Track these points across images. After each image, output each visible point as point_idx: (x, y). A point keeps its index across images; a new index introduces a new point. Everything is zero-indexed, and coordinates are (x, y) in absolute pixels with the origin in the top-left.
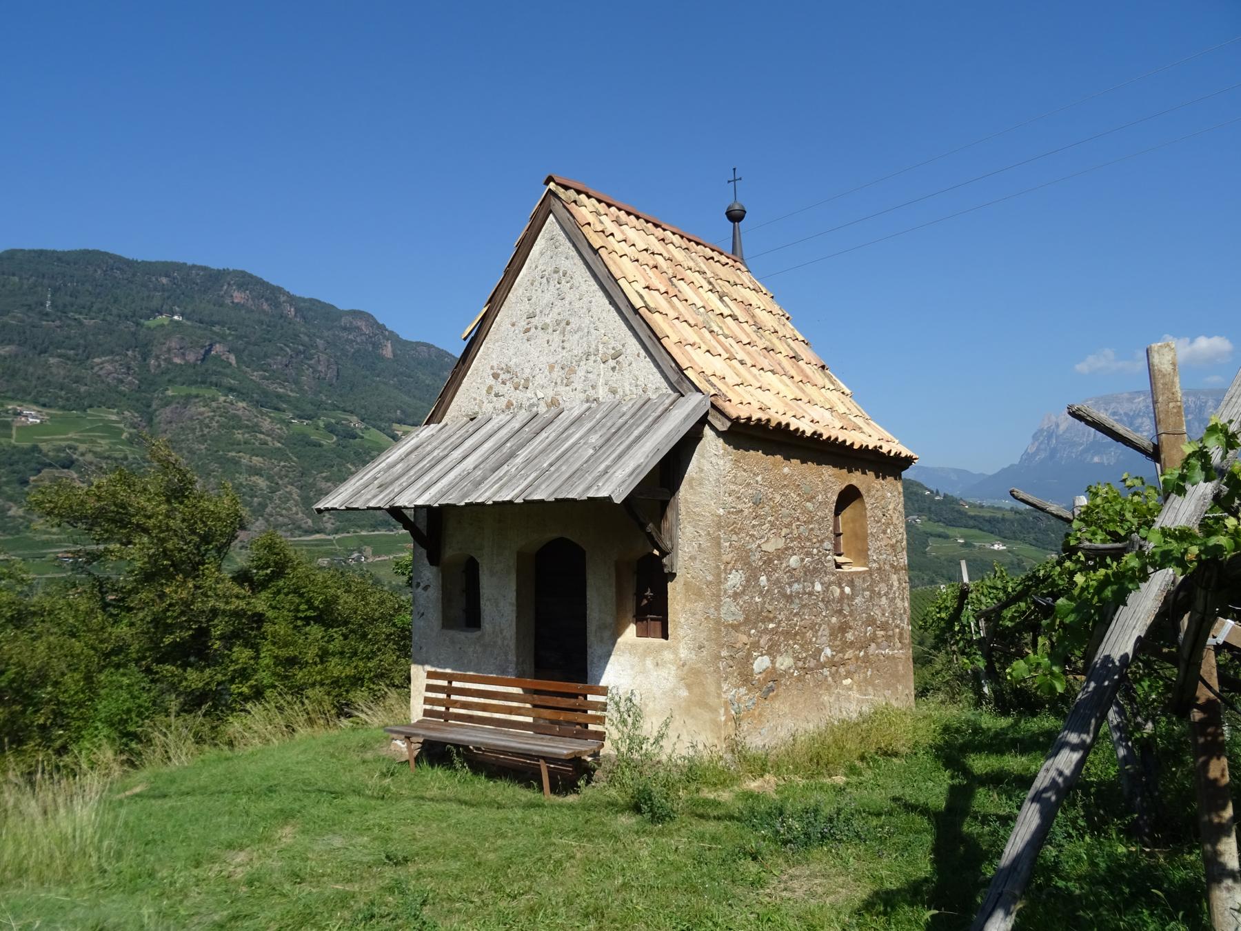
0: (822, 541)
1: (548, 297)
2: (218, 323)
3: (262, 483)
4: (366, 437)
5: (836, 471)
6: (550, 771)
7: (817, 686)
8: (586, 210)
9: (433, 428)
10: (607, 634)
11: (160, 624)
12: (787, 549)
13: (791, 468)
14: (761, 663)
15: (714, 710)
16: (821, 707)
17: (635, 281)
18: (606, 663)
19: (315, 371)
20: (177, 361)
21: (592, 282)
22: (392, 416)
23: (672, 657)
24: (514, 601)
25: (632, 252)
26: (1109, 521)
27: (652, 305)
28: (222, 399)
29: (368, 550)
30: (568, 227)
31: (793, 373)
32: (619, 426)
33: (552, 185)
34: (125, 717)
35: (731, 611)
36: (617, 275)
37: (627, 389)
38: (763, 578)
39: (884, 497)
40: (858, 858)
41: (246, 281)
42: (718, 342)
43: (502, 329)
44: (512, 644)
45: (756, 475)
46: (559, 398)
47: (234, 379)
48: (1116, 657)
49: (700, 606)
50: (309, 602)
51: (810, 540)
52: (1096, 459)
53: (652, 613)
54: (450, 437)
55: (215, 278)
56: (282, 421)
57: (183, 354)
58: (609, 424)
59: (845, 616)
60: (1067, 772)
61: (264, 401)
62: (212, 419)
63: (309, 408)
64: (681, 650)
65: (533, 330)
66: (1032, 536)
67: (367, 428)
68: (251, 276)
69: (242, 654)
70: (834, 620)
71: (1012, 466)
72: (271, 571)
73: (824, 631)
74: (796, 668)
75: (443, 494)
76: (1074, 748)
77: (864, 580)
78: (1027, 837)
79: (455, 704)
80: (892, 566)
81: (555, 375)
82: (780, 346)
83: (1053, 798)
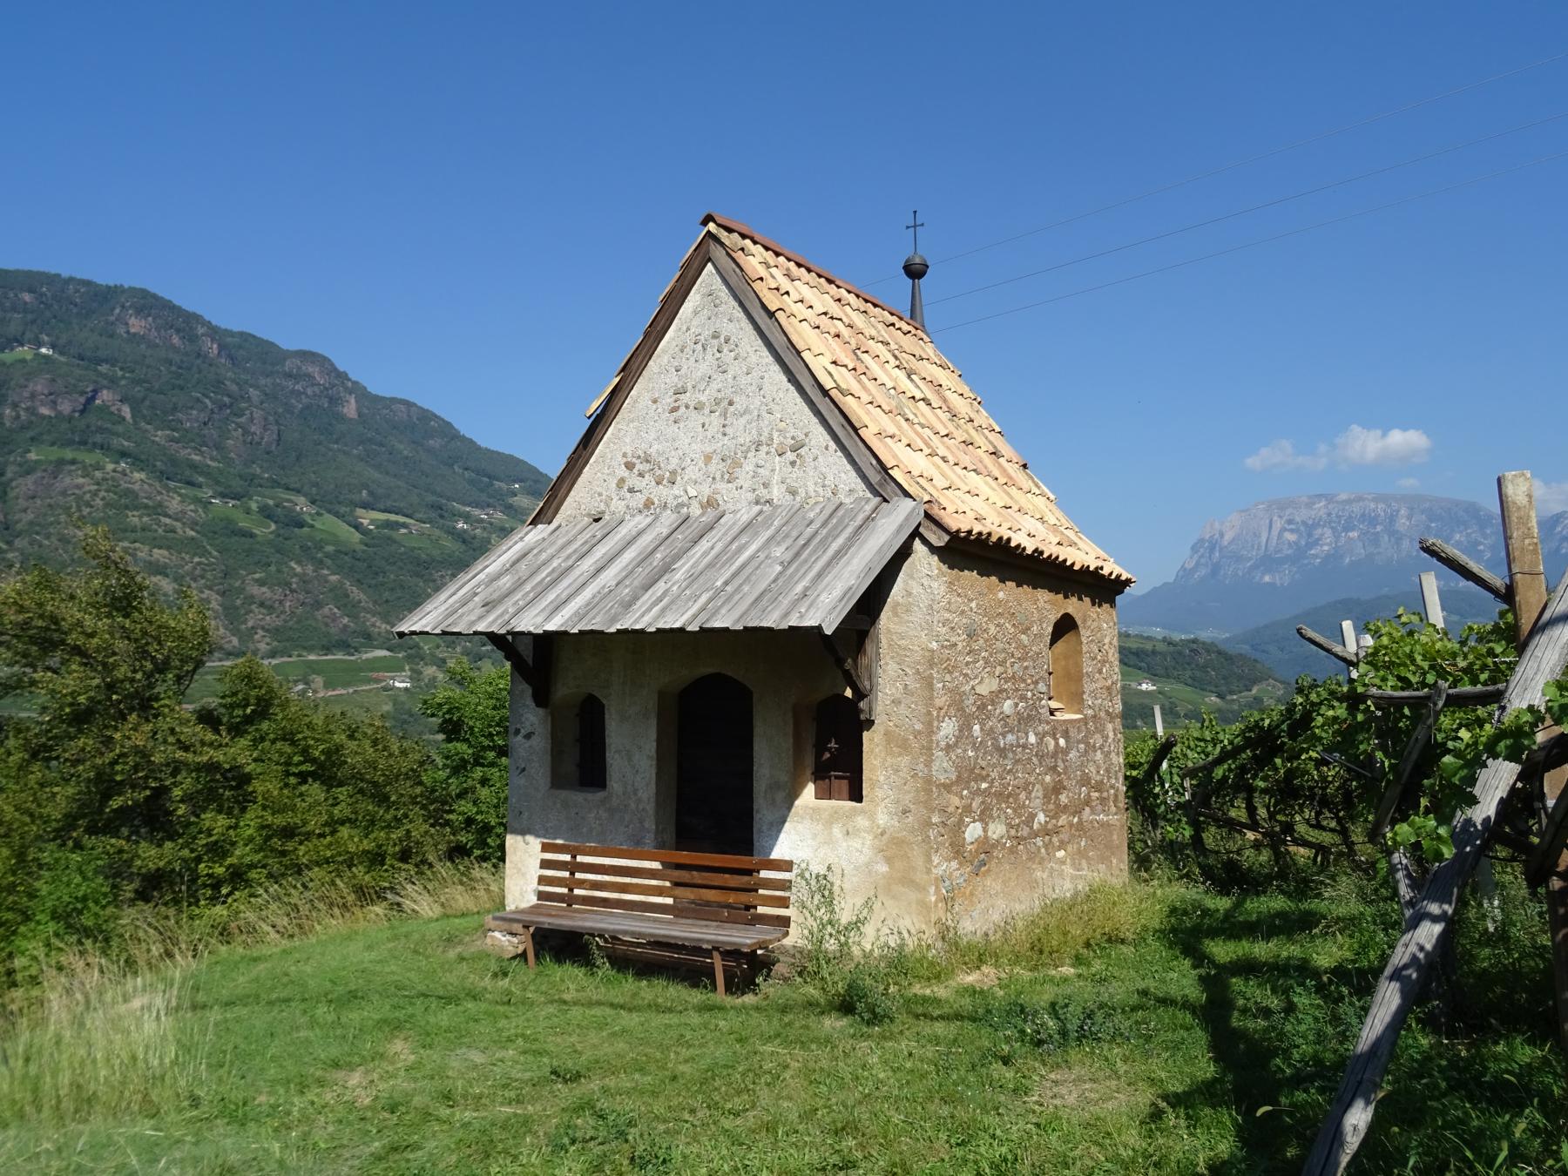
0: (1036, 683)
1: (704, 368)
2: (106, 361)
3: (167, 585)
4: (318, 525)
5: (1051, 596)
6: (726, 970)
7: (1029, 859)
8: (754, 259)
9: (542, 530)
10: (780, 796)
11: (106, 785)
12: (1001, 691)
13: (1006, 592)
14: (973, 831)
15: (922, 889)
16: (1033, 884)
17: (821, 356)
18: (779, 831)
19: (246, 432)
20: (45, 411)
21: (765, 352)
22: (356, 497)
23: (867, 823)
24: (653, 752)
25: (808, 314)
26: (1399, 665)
27: (844, 386)
28: (110, 467)
29: (318, 681)
30: (733, 281)
31: (996, 473)
32: (813, 537)
33: (711, 226)
34: (79, 906)
35: (943, 769)
36: (800, 347)
37: (811, 488)
38: (977, 727)
39: (1100, 629)
40: (1125, 1060)
41: (147, 303)
42: (917, 433)
43: (639, 406)
44: (650, 808)
45: (971, 600)
46: (718, 497)
47: (128, 439)
48: (1478, 821)
49: (905, 761)
50: (305, 751)
51: (1024, 681)
52: (1267, 579)
53: (842, 771)
54: (570, 542)
55: (102, 298)
56: (197, 501)
57: (54, 402)
58: (795, 534)
59: (1059, 774)
60: (1429, 947)
61: (171, 472)
62: (95, 494)
63: (237, 485)
64: (880, 816)
65: (683, 409)
66: (1188, 673)
67: (318, 514)
68: (155, 296)
69: (214, 821)
70: (1048, 778)
71: (1165, 584)
72: (251, 709)
73: (1038, 792)
74: (1009, 838)
75: (580, 616)
76: (1435, 919)
77: (1079, 731)
78: (1388, 1019)
79: (582, 884)
80: (1108, 713)
81: (712, 468)
82: (979, 439)
83: (1414, 976)
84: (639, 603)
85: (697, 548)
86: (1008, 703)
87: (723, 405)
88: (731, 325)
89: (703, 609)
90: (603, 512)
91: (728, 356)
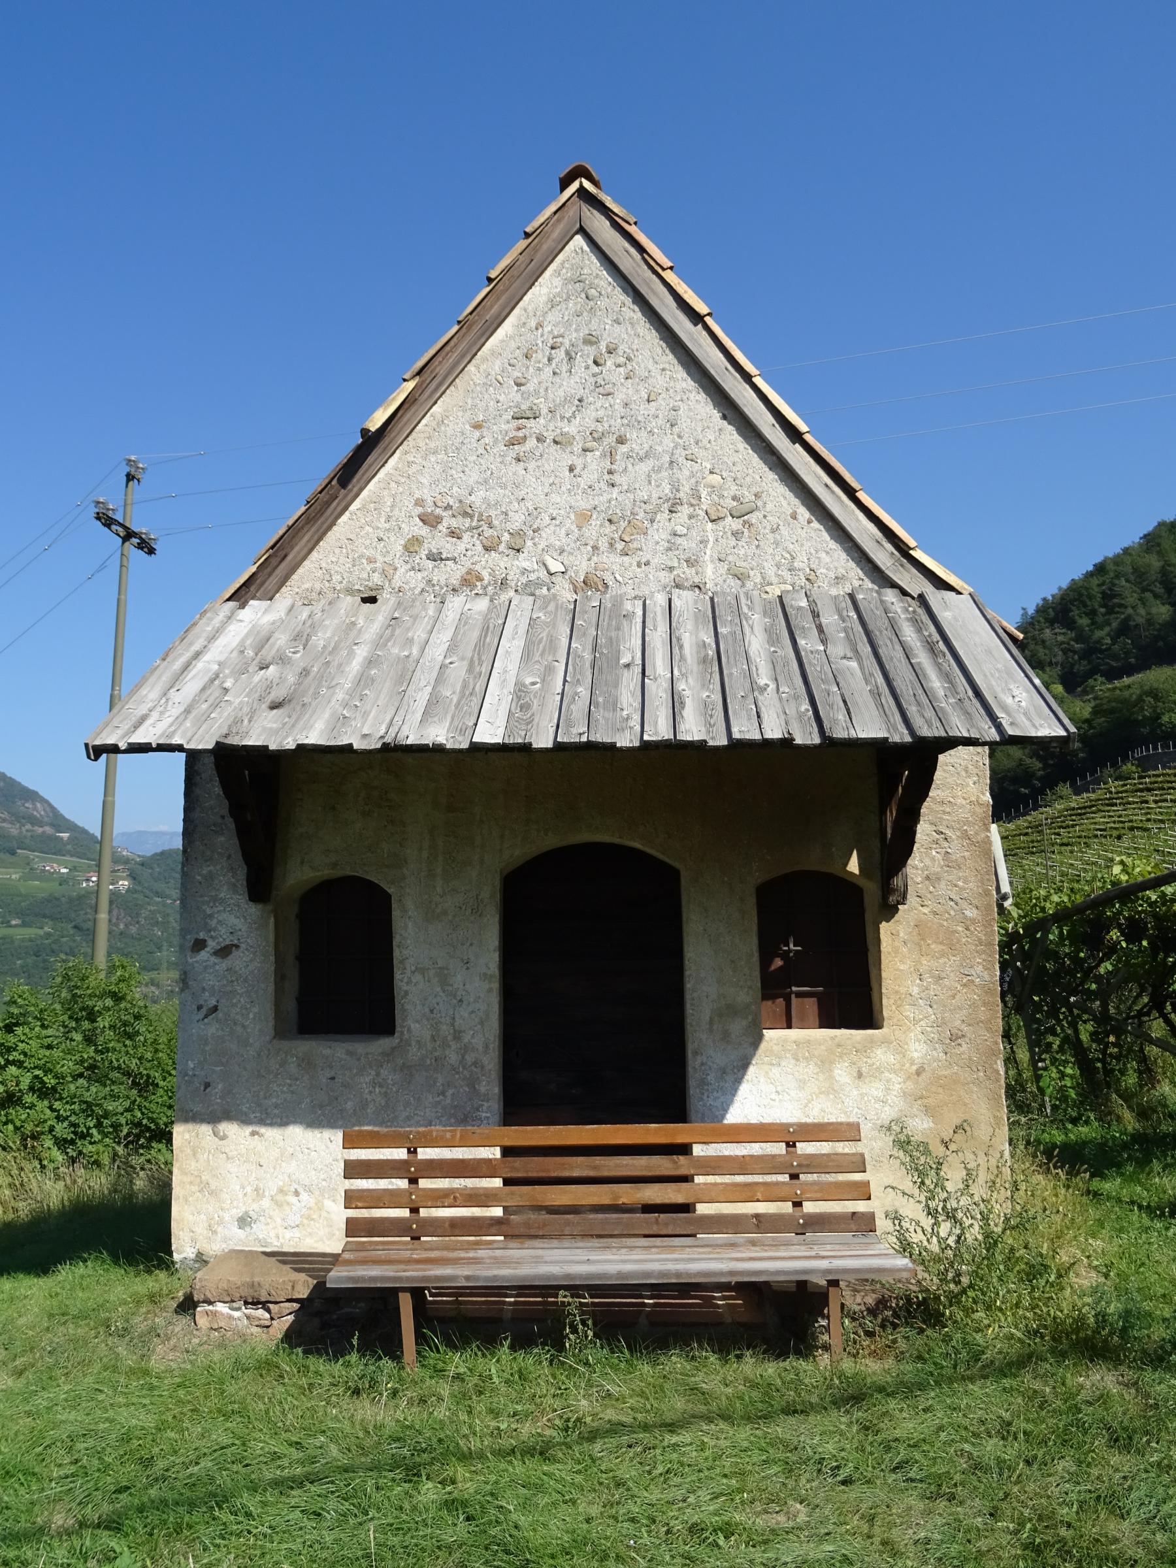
10: (737, 1026)
18: (739, 1081)
37: (771, 573)
49: (949, 964)
65: (532, 443)
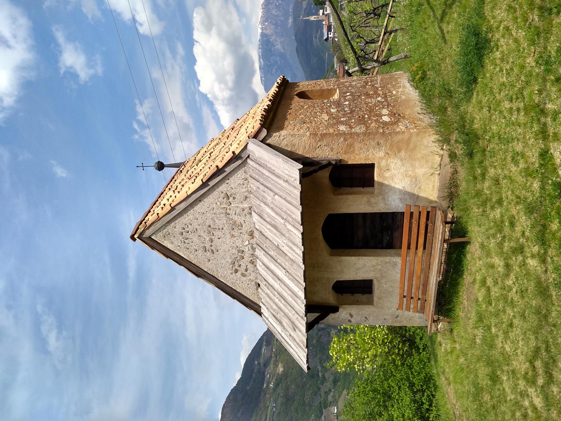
0: (324, 103)
1: (195, 239)
12: (327, 113)
14: (386, 119)
15: (411, 134)
37: (245, 190)
38: (342, 119)
44: (381, 259)
45: (290, 123)
54: (268, 296)
65: (212, 248)
80: (337, 81)
84: (292, 257)
85: (269, 237)
86: (332, 110)
87: (210, 229)
88: (177, 227)
89: (294, 226)
90: (256, 283)
91: (190, 228)
